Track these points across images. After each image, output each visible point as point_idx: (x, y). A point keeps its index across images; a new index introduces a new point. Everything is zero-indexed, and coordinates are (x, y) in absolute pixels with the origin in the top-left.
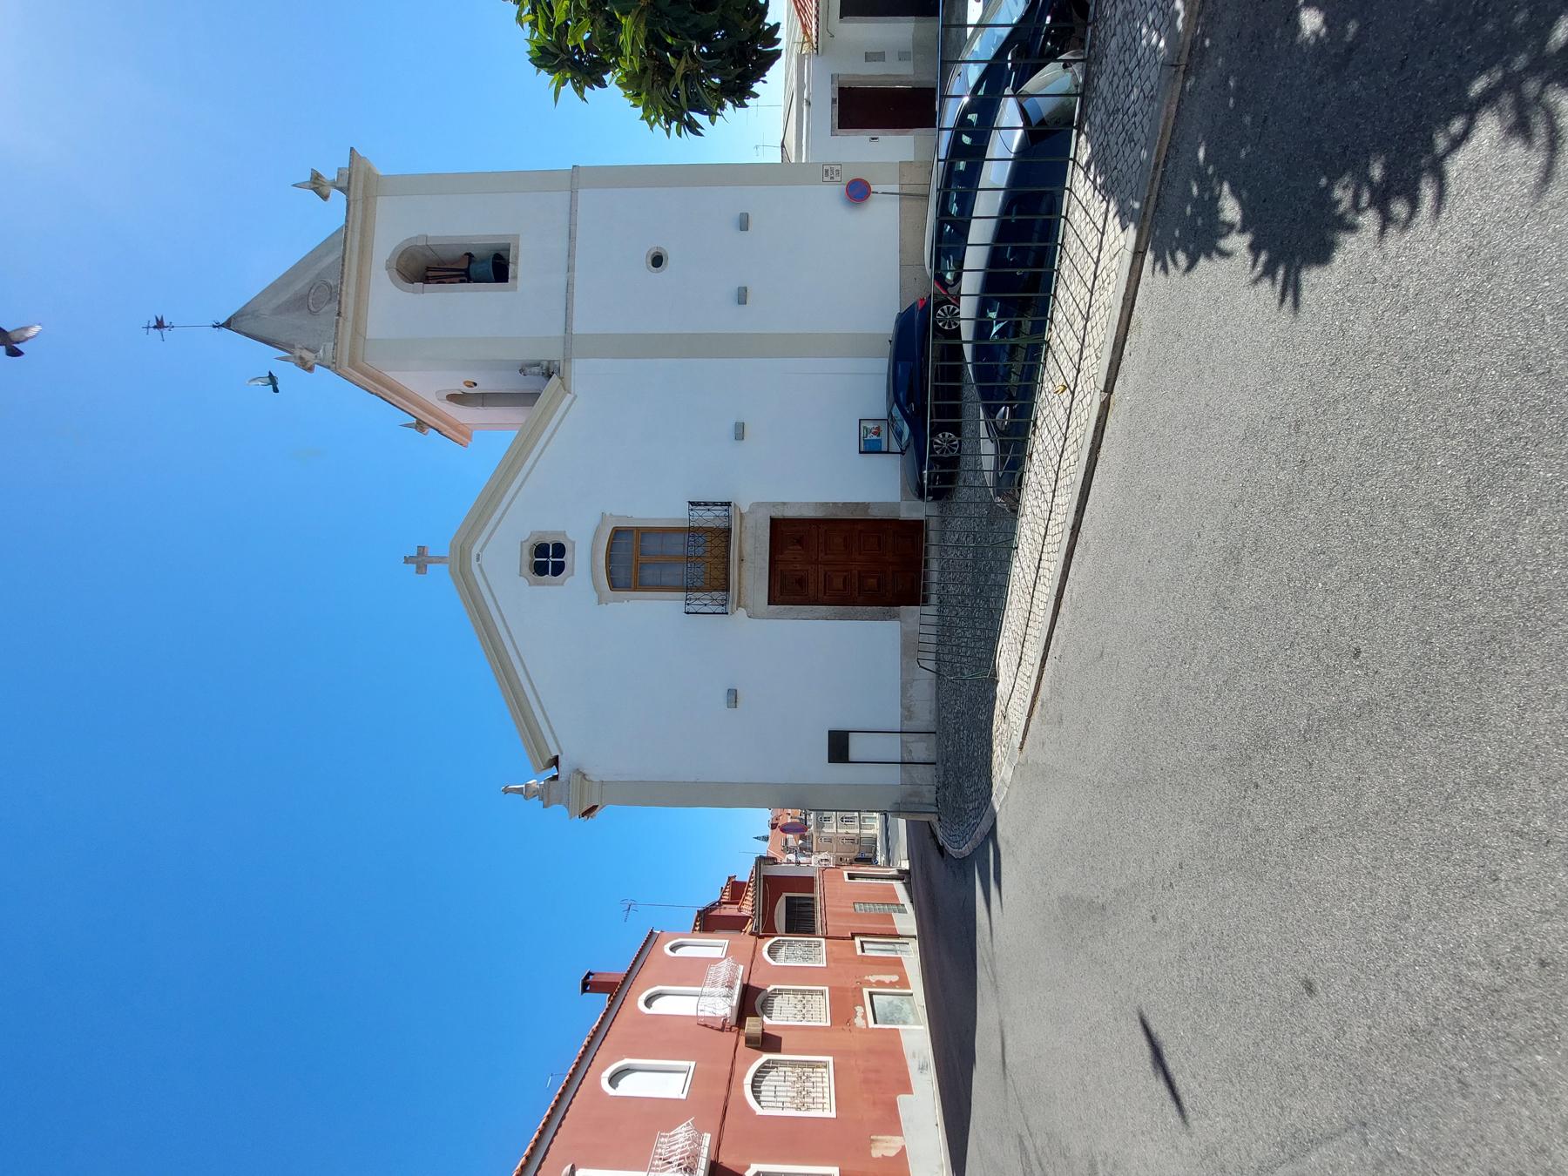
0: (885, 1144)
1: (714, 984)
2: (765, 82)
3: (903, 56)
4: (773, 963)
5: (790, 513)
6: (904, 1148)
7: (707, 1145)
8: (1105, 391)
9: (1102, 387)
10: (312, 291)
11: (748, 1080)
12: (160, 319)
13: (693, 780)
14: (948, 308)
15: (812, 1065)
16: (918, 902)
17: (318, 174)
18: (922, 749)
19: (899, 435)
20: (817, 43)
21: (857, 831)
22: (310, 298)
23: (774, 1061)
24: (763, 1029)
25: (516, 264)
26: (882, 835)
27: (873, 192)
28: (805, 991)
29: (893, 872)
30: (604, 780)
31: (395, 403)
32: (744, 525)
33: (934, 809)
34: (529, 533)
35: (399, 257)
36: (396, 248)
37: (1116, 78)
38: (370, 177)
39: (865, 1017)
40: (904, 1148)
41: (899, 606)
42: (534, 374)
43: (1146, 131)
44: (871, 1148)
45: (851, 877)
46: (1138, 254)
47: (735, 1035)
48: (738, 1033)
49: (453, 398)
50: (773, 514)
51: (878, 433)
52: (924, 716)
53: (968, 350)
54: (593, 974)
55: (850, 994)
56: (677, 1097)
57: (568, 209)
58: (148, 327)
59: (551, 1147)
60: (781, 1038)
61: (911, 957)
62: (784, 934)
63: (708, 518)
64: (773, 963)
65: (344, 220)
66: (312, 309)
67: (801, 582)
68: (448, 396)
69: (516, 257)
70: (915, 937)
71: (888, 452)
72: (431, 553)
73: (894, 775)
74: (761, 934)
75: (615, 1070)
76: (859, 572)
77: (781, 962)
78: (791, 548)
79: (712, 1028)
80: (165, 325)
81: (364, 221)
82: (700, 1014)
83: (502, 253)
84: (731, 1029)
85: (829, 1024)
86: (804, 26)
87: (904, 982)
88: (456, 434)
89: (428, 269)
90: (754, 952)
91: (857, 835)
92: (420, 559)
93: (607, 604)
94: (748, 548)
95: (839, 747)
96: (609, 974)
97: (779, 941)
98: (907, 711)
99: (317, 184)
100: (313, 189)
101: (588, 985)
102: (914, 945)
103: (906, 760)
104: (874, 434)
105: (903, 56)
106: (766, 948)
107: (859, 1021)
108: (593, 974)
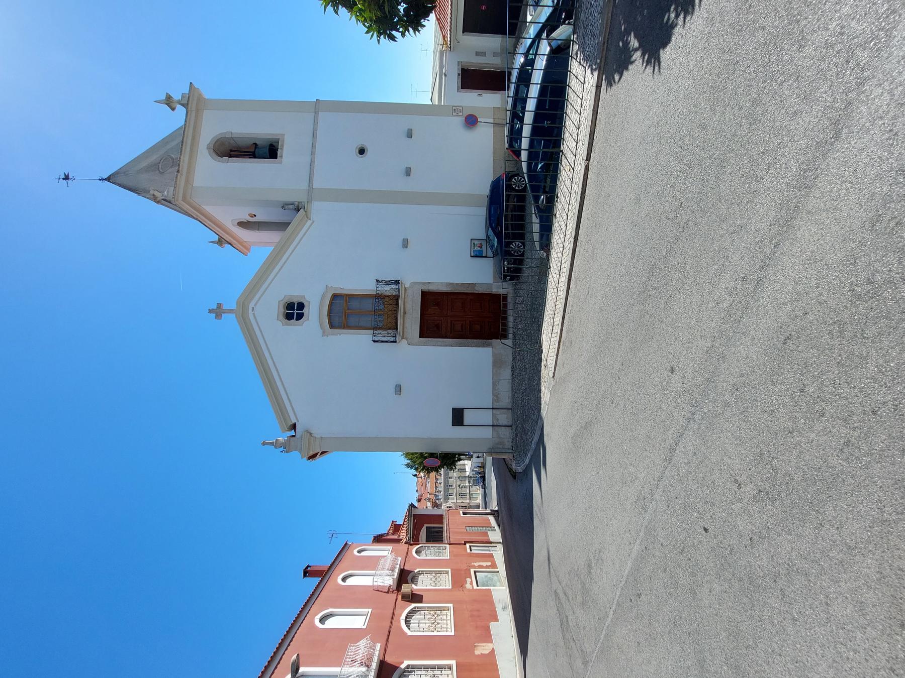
0: (483, 648)
1: (383, 569)
2: (428, 20)
3: (495, 55)
4: (418, 557)
5: (432, 288)
6: (493, 649)
7: (378, 649)
8: (587, 160)
9: (585, 159)
10: (162, 161)
11: (403, 617)
12: (67, 174)
14: (518, 178)
15: (441, 609)
16: (503, 524)
17: (170, 95)
18: (505, 418)
19: (492, 247)
20: (450, 45)
21: (468, 501)
22: (160, 165)
23: (418, 608)
24: (412, 591)
25: (282, 149)
26: (482, 504)
27: (479, 122)
28: (437, 571)
29: (488, 511)
30: (323, 436)
31: (207, 225)
32: (406, 294)
33: (511, 451)
34: (283, 296)
35: (215, 143)
36: (212, 139)
37: (587, 11)
38: (200, 99)
39: (471, 583)
40: (493, 649)
41: (492, 339)
42: (290, 209)
43: (599, 29)
44: (474, 650)
45: (464, 513)
46: (598, 87)
47: (395, 595)
48: (398, 594)
49: (242, 224)
51: (480, 246)
52: (506, 400)
53: (526, 176)
54: (310, 567)
55: (463, 572)
56: (360, 628)
57: (313, 121)
58: (59, 179)
59: (283, 657)
60: (422, 596)
61: (498, 554)
62: (425, 542)
63: (387, 289)
64: (418, 557)
65: (184, 121)
66: (161, 170)
67: (438, 327)
68: (238, 223)
69: (282, 146)
70: (500, 543)
71: (486, 257)
72: (224, 307)
73: (488, 433)
74: (411, 543)
75: (321, 616)
77: (422, 557)
78: (433, 308)
79: (382, 591)
80: (70, 178)
81: (196, 123)
82: (375, 584)
83: (274, 144)
84: (393, 592)
85: (450, 587)
86: (444, 37)
87: (494, 565)
88: (241, 247)
89: (231, 151)
90: (407, 554)
91: (468, 503)
92: (218, 311)
93: (327, 336)
94: (408, 307)
95: (458, 417)
96: (320, 566)
97: (422, 546)
98: (496, 398)
99: (169, 102)
100: (167, 104)
101: (307, 573)
102: (500, 547)
103: (495, 424)
104: (479, 247)
105: (495, 55)
106: (414, 550)
107: (468, 586)
108: (310, 567)
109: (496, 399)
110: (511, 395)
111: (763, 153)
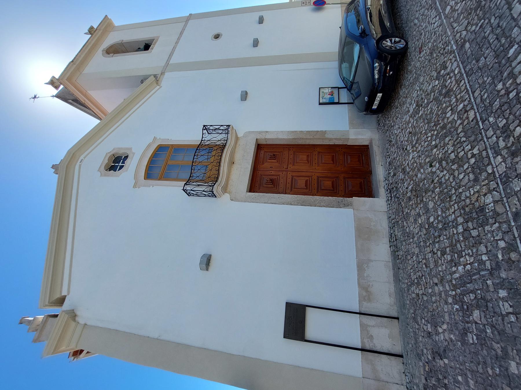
13: (156, 336)
25: (154, 44)
30: (89, 323)
50: (258, 138)
63: (216, 138)
71: (338, 103)
76: (318, 177)
93: (139, 188)
103: (368, 347)
109: (364, 294)
110: (393, 289)
111: (434, 302)
